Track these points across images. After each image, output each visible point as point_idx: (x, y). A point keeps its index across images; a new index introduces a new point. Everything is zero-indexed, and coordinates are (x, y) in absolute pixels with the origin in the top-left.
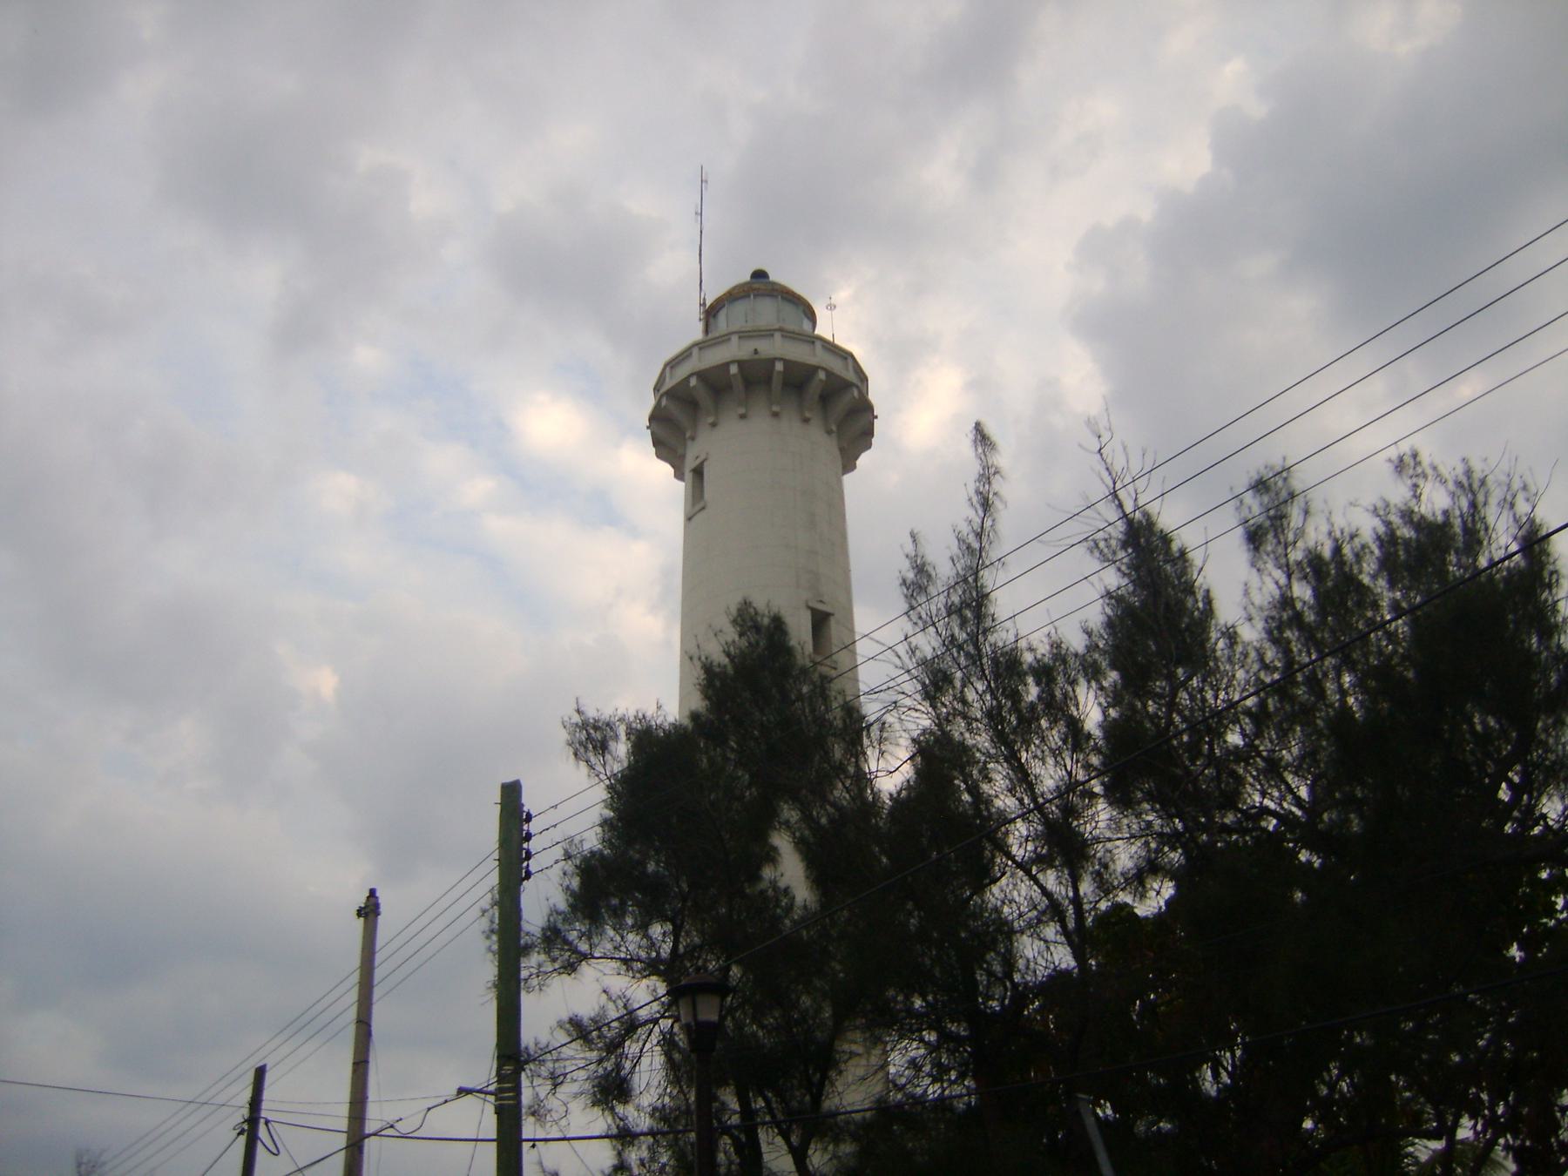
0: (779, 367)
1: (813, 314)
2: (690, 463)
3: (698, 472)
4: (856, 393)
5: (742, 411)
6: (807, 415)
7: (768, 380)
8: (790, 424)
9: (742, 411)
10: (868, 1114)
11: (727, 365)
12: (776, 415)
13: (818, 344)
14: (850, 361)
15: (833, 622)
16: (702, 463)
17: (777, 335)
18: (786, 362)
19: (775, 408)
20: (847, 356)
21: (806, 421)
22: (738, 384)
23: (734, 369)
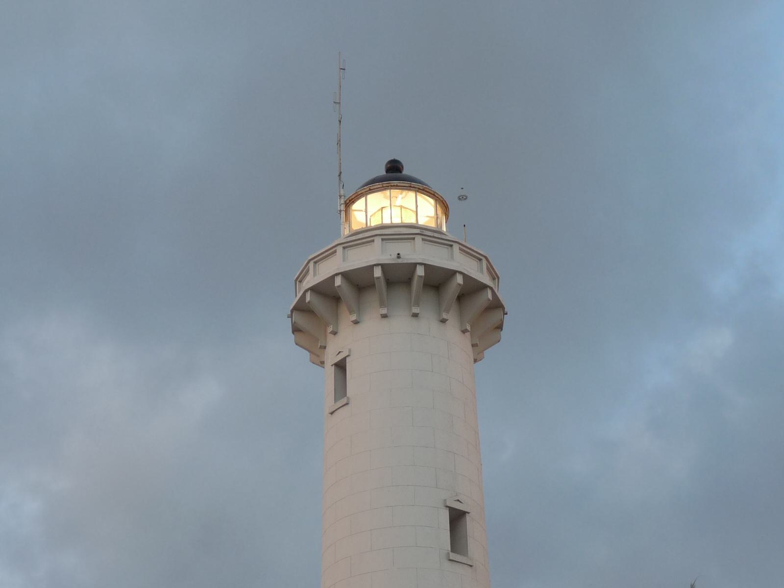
0: (420, 271)
1: (487, 269)
2: (331, 358)
3: (341, 366)
4: (490, 296)
5: (384, 311)
6: (445, 316)
7: (408, 282)
8: (428, 323)
9: (384, 311)
10: (438, 206)
11: (371, 268)
12: (415, 315)
13: (456, 247)
14: (484, 262)
15: (468, 517)
16: (344, 360)
17: (418, 239)
18: (427, 267)
19: (415, 310)
20: (403, 167)
21: (444, 321)
22: (383, 284)
23: (378, 273)
